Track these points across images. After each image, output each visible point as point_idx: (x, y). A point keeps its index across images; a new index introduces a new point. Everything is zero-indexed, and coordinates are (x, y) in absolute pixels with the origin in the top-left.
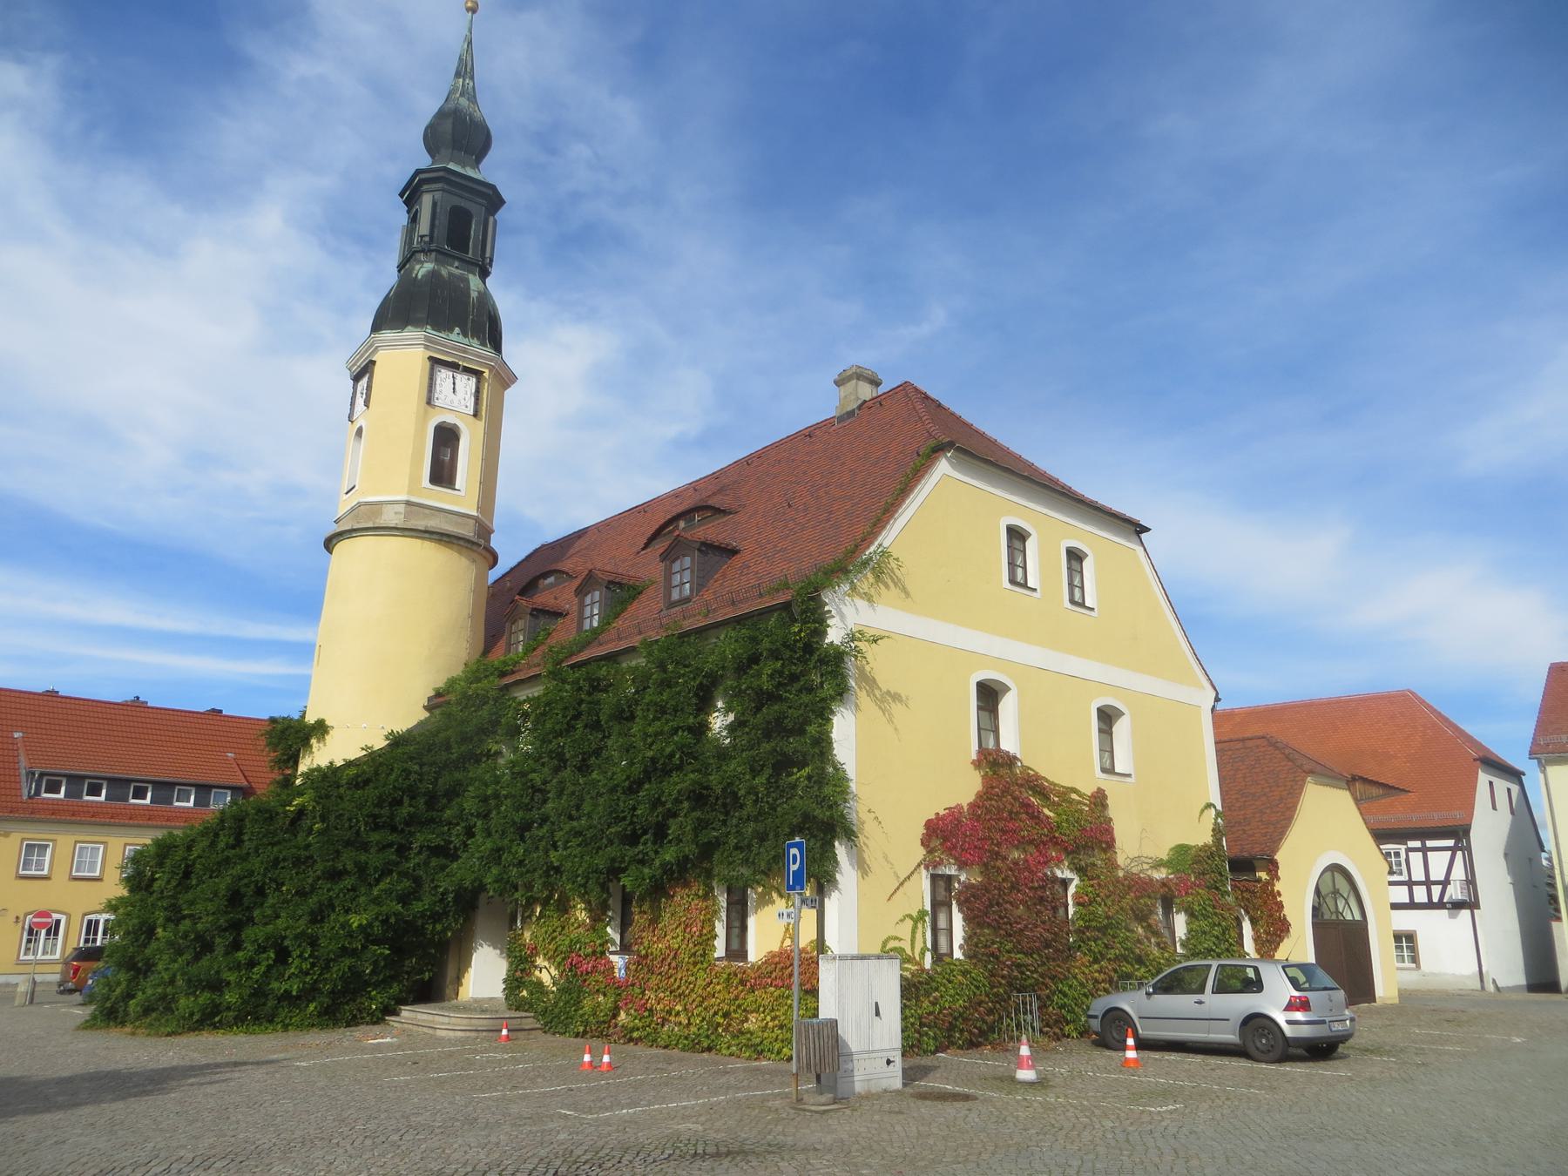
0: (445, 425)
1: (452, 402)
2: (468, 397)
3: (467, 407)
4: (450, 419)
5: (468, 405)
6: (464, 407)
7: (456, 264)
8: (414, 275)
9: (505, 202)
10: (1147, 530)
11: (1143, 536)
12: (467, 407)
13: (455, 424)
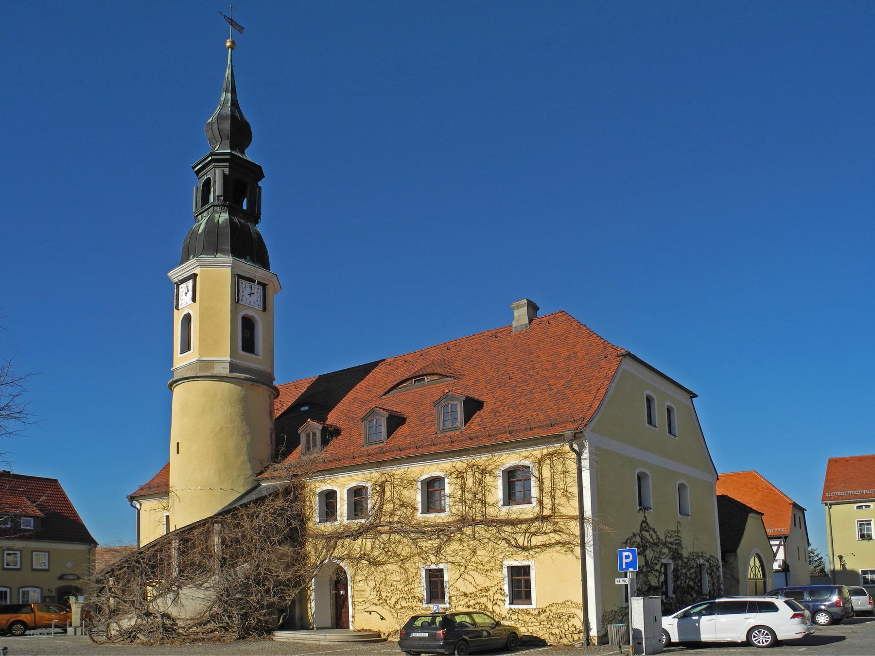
0: (245, 316)
1: (250, 302)
2: (259, 299)
3: (259, 305)
4: (250, 313)
5: (260, 304)
6: (257, 306)
7: (241, 215)
8: (216, 221)
9: (263, 176)
10: (695, 396)
11: (694, 399)
12: (259, 305)
13: (253, 316)
